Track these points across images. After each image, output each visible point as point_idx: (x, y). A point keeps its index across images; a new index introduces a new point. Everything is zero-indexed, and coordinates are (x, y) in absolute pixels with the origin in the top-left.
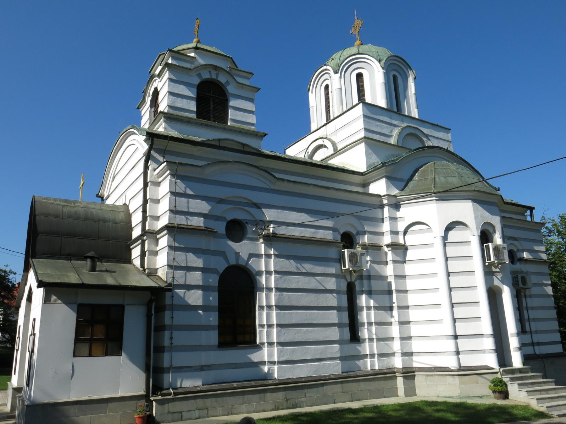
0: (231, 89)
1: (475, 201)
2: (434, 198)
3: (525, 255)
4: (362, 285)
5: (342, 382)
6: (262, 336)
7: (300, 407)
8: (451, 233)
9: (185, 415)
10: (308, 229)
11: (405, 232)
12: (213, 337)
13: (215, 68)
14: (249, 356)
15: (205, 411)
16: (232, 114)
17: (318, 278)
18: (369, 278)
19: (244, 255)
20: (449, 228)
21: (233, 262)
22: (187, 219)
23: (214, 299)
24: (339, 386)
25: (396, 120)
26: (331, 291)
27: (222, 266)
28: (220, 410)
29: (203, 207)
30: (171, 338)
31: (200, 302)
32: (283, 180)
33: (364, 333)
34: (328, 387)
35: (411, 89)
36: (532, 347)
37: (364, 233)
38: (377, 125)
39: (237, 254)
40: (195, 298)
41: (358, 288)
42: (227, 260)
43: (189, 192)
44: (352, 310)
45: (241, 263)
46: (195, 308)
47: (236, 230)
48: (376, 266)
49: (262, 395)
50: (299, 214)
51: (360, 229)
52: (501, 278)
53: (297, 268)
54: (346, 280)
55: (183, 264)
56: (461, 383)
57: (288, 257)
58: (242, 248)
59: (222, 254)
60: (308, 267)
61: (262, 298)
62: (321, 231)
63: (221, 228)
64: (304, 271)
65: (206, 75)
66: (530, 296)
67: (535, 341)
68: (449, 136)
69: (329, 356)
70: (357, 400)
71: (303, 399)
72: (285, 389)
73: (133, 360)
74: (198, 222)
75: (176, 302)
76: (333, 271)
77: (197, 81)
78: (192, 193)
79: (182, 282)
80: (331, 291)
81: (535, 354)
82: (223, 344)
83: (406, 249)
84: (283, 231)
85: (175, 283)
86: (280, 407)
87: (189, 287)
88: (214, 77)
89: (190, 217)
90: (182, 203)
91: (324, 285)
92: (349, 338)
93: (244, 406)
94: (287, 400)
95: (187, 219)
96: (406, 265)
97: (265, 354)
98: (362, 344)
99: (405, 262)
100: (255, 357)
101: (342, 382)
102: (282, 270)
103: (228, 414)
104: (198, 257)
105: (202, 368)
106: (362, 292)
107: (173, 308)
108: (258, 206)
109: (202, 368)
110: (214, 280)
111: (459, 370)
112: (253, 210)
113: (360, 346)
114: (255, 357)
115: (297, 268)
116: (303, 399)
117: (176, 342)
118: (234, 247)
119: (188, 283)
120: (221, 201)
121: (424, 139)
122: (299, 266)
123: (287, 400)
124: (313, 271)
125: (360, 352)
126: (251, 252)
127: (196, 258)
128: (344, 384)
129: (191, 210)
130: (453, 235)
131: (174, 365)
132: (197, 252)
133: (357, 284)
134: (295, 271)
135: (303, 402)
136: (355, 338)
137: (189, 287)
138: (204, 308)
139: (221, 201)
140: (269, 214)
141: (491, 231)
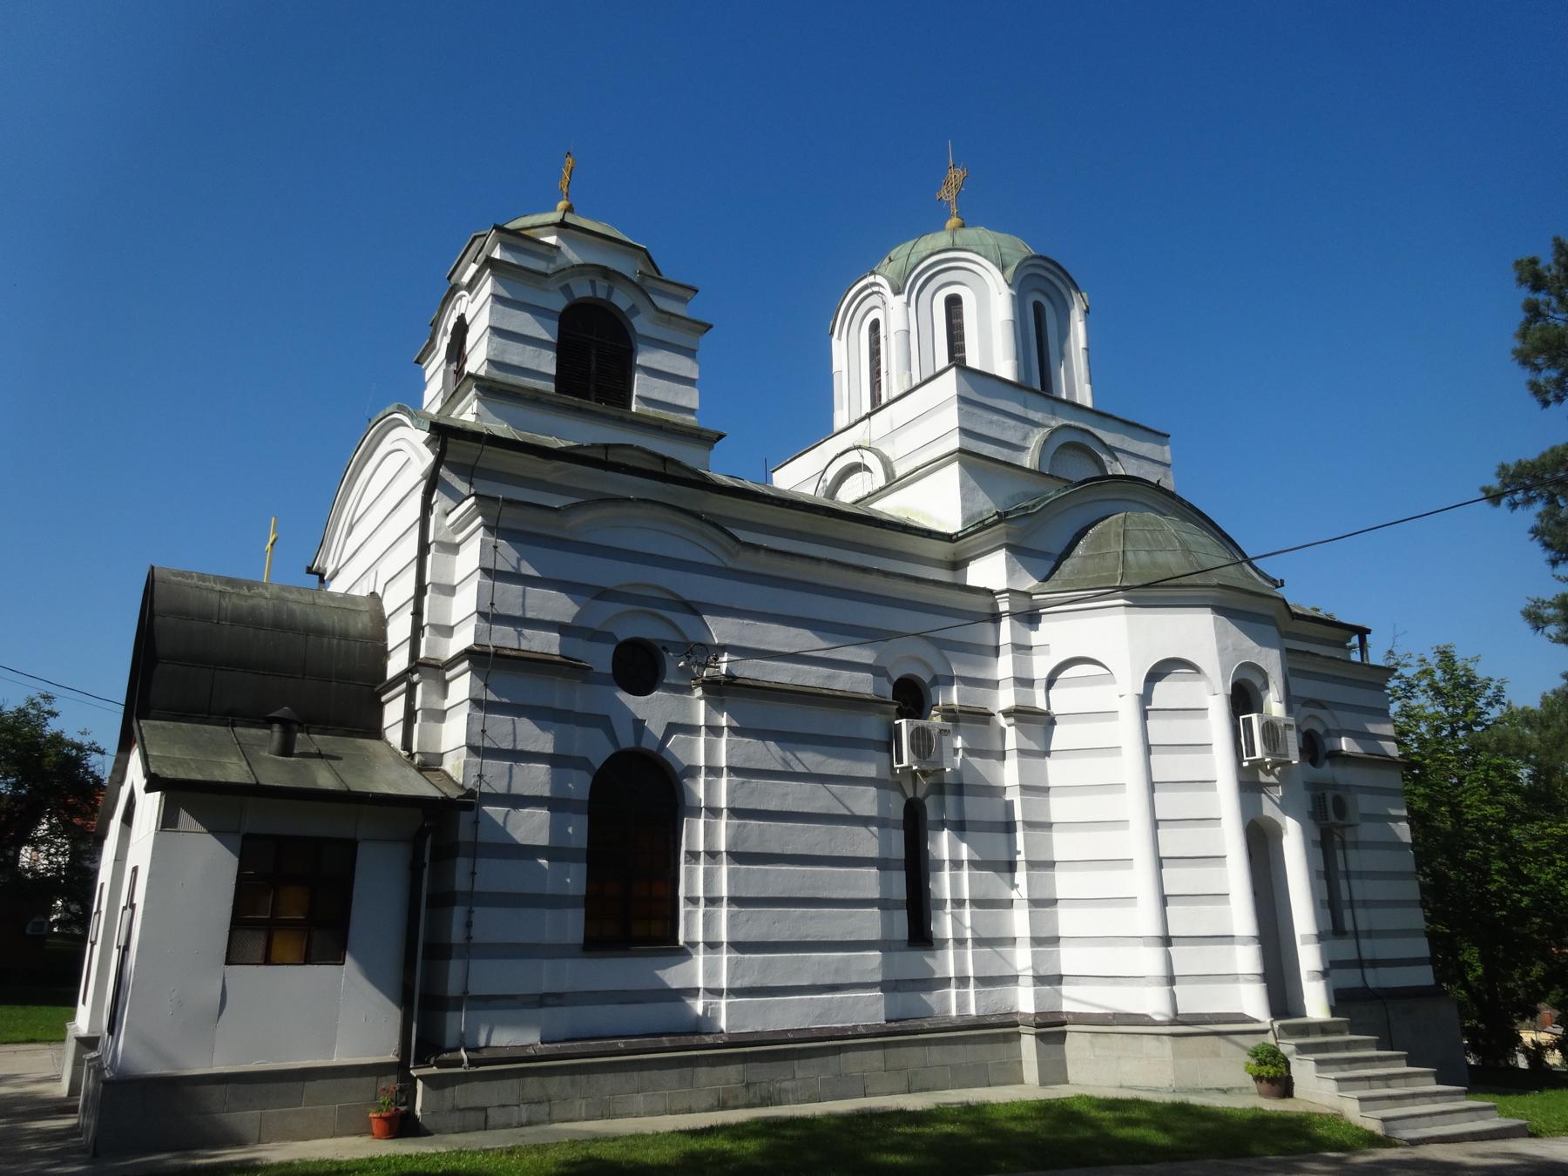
0: (642, 324)
1: (1219, 610)
2: (1122, 602)
3: (1345, 744)
4: (941, 807)
5: (885, 1045)
6: (692, 925)
7: (780, 1103)
8: (1159, 687)
9: (495, 1115)
10: (815, 668)
11: (1050, 682)
12: (572, 926)
13: (606, 273)
14: (658, 972)
15: (544, 1108)
16: (641, 385)
17: (835, 787)
18: (959, 790)
19: (656, 728)
20: (1157, 673)
21: (627, 742)
22: (520, 634)
23: (577, 830)
24: (878, 1053)
26: (865, 821)
27: (599, 750)
28: (580, 1106)
29: (561, 606)
30: (469, 925)
31: (543, 839)
32: (756, 548)
33: (944, 925)
34: (850, 1055)
35: (1076, 336)
36: (1358, 971)
37: (949, 681)
38: (991, 422)
39: (639, 725)
40: (531, 827)
41: (931, 815)
42: (613, 738)
43: (527, 569)
44: (917, 867)
45: (647, 744)
46: (532, 852)
47: (640, 667)
48: (976, 762)
49: (686, 1071)
50: (794, 631)
51: (940, 671)
52: (1281, 798)
53: (785, 762)
54: (904, 794)
55: (506, 745)
56: (1176, 1054)
57: (762, 734)
58: (653, 709)
59: (603, 722)
60: (811, 760)
61: (695, 833)
62: (846, 674)
63: (601, 658)
64: (800, 769)
65: (582, 290)
66: (1356, 845)
67: (1366, 955)
68: (1165, 453)
69: (854, 980)
70: (921, 1090)
71: (787, 1085)
72: (745, 1058)
73: (372, 976)
74: (546, 643)
75: (484, 836)
76: (871, 770)
77: (559, 303)
79: (500, 787)
80: (865, 821)
81: (1366, 988)
82: (597, 943)
83: (1052, 722)
84: (751, 670)
85: (485, 789)
86: (730, 1103)
87: (516, 801)
88: (601, 294)
89: (526, 632)
91: (847, 803)
93: (640, 1097)
94: (748, 1086)
95: (520, 634)
96: (1049, 762)
97: (696, 972)
98: (939, 953)
99: (1047, 753)
100: (673, 977)
101: (885, 1045)
102: (747, 765)
103: (602, 1117)
104: (543, 729)
105: (542, 1000)
106: (941, 825)
107: (478, 850)
108: (694, 609)
109: (542, 1000)
110: (579, 786)
111: (1173, 1023)
112: (680, 619)
113: (934, 957)
114: (673, 977)
115: (785, 762)
116: (787, 1085)
117: (479, 936)
118: (632, 707)
119: (514, 791)
120: (603, 594)
121: (1104, 457)
122: (789, 756)
123: (748, 1086)
124: (821, 770)
125: (933, 972)
126: (674, 719)
127: (537, 731)
128: (890, 1051)
129: (529, 615)
130: (1165, 693)
131: (473, 991)
132: (541, 715)
133: (930, 803)
134: (779, 768)
135: (786, 1091)
136: (921, 936)
137: (516, 801)
139: (603, 594)
140: (720, 629)
141: (1258, 683)
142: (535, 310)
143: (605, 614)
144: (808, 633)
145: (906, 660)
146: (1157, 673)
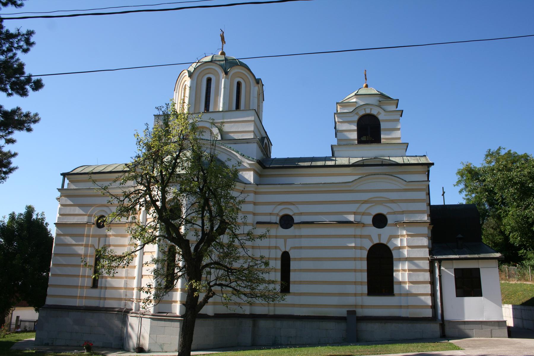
0: (380, 117)
25: (249, 116)
27: (368, 245)
42: (371, 240)
59: (369, 237)
63: (369, 220)
65: (362, 113)
77: (356, 118)
78: (71, 203)
90: (68, 210)
139: (365, 202)
142: (350, 122)
143: (364, 208)
144: (77, 208)
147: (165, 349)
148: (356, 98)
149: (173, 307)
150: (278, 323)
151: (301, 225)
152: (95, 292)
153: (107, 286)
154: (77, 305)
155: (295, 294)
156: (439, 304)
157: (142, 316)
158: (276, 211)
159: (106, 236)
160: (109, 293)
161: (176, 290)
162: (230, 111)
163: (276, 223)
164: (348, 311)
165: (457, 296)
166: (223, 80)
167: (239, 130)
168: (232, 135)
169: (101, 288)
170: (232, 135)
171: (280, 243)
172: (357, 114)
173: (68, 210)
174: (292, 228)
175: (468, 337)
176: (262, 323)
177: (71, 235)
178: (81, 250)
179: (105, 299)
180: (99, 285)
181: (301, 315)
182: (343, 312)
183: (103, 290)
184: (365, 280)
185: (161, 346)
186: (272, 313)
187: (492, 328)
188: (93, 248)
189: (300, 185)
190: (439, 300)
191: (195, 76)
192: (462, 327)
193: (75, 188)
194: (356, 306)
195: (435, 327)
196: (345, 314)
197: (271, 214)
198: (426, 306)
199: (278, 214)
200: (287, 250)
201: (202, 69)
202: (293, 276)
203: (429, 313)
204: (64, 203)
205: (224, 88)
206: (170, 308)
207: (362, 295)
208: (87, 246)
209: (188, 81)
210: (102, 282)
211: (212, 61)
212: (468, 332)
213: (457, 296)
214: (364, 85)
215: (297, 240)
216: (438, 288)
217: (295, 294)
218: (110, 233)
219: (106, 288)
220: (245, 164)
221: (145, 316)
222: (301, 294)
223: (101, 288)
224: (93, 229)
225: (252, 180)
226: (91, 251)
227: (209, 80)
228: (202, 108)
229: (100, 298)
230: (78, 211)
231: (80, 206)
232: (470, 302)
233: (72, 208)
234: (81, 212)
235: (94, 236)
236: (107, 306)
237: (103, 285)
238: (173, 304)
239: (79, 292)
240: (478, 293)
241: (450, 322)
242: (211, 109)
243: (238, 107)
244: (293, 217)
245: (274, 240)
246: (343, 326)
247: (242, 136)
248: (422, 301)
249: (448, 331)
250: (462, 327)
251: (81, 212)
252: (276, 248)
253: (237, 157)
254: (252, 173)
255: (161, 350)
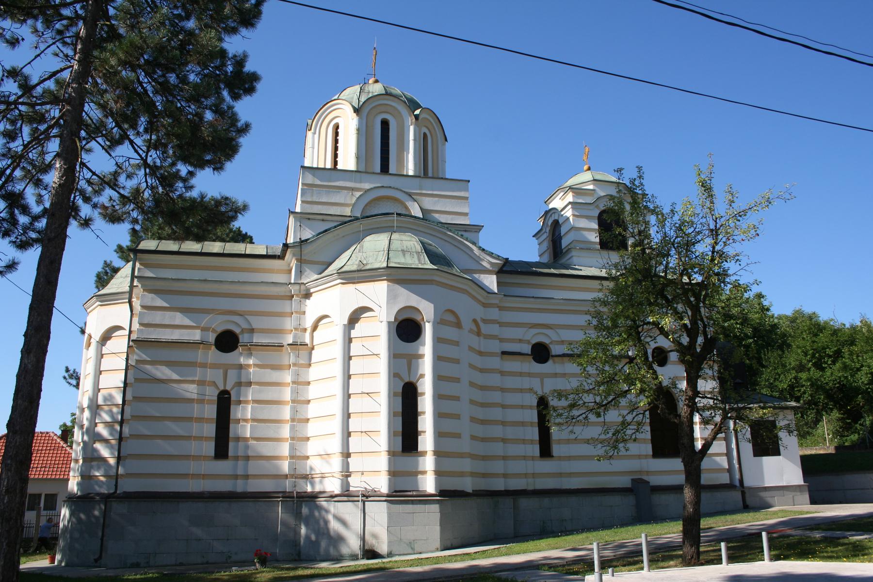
2: (339, 281)
11: (315, 328)
12: (648, 449)
20: (354, 318)
46: (190, 401)
51: (245, 326)
77: (596, 213)
78: (165, 305)
83: (313, 348)
90: (158, 317)
92: (651, 453)
138: (201, 401)
141: (418, 318)
142: (588, 217)
144: (178, 314)
145: (221, 324)
146: (354, 318)
147: (417, 549)
148: (594, 185)
149: (420, 481)
150: (546, 501)
151: (566, 359)
152: (223, 467)
153: (250, 453)
154: (190, 490)
155: (560, 458)
156: (737, 466)
157: (364, 498)
158: (527, 338)
159: (241, 367)
160: (253, 468)
161: (424, 454)
162: (419, 177)
163: (527, 355)
164: (633, 480)
165: (755, 455)
166: (412, 128)
167: (447, 210)
168: (436, 216)
169: (237, 458)
170: (436, 216)
171: (536, 384)
172: (597, 207)
173: (158, 317)
174: (550, 362)
175: (770, 506)
176: (525, 503)
177: (169, 364)
178: (191, 390)
179: (246, 477)
180: (230, 453)
181: (573, 488)
182: (624, 482)
183: (241, 463)
184: (650, 437)
185: (411, 544)
186: (531, 488)
187: (794, 493)
188: (213, 388)
189: (562, 301)
190: (735, 462)
191: (365, 111)
192: (763, 494)
193: (151, 275)
194: (640, 472)
195: (737, 495)
196: (629, 485)
197: (520, 341)
198: (722, 470)
199: (528, 342)
200: (228, 388)
201: (373, 105)
202: (534, 433)
203: (725, 479)
204: (149, 304)
205: (415, 140)
206: (416, 482)
207: (646, 456)
208: (201, 383)
209: (349, 123)
210: (236, 448)
211: (387, 94)
212: (769, 500)
213: (755, 455)
214: (586, 167)
215: (559, 380)
216: (734, 446)
217: (560, 458)
218: (251, 362)
219: (247, 458)
220: (485, 264)
221: (370, 499)
222: (569, 458)
223: (237, 458)
224: (214, 355)
225: (495, 289)
226: (212, 394)
227: (385, 124)
228: (378, 169)
229: (236, 477)
230: (179, 319)
231: (184, 311)
232: (768, 462)
233: (168, 314)
234: (187, 322)
235: (214, 366)
236: (251, 489)
237: (241, 453)
238: (420, 476)
239: (193, 467)
240: (777, 453)
241: (750, 488)
242: (392, 169)
243: (426, 175)
244: (551, 346)
245: (527, 379)
246: (631, 500)
247: (452, 219)
248: (716, 462)
249: (749, 501)
250: (763, 494)
251: (187, 322)
252: (531, 390)
253: (472, 250)
254: (494, 278)
255: (410, 551)
